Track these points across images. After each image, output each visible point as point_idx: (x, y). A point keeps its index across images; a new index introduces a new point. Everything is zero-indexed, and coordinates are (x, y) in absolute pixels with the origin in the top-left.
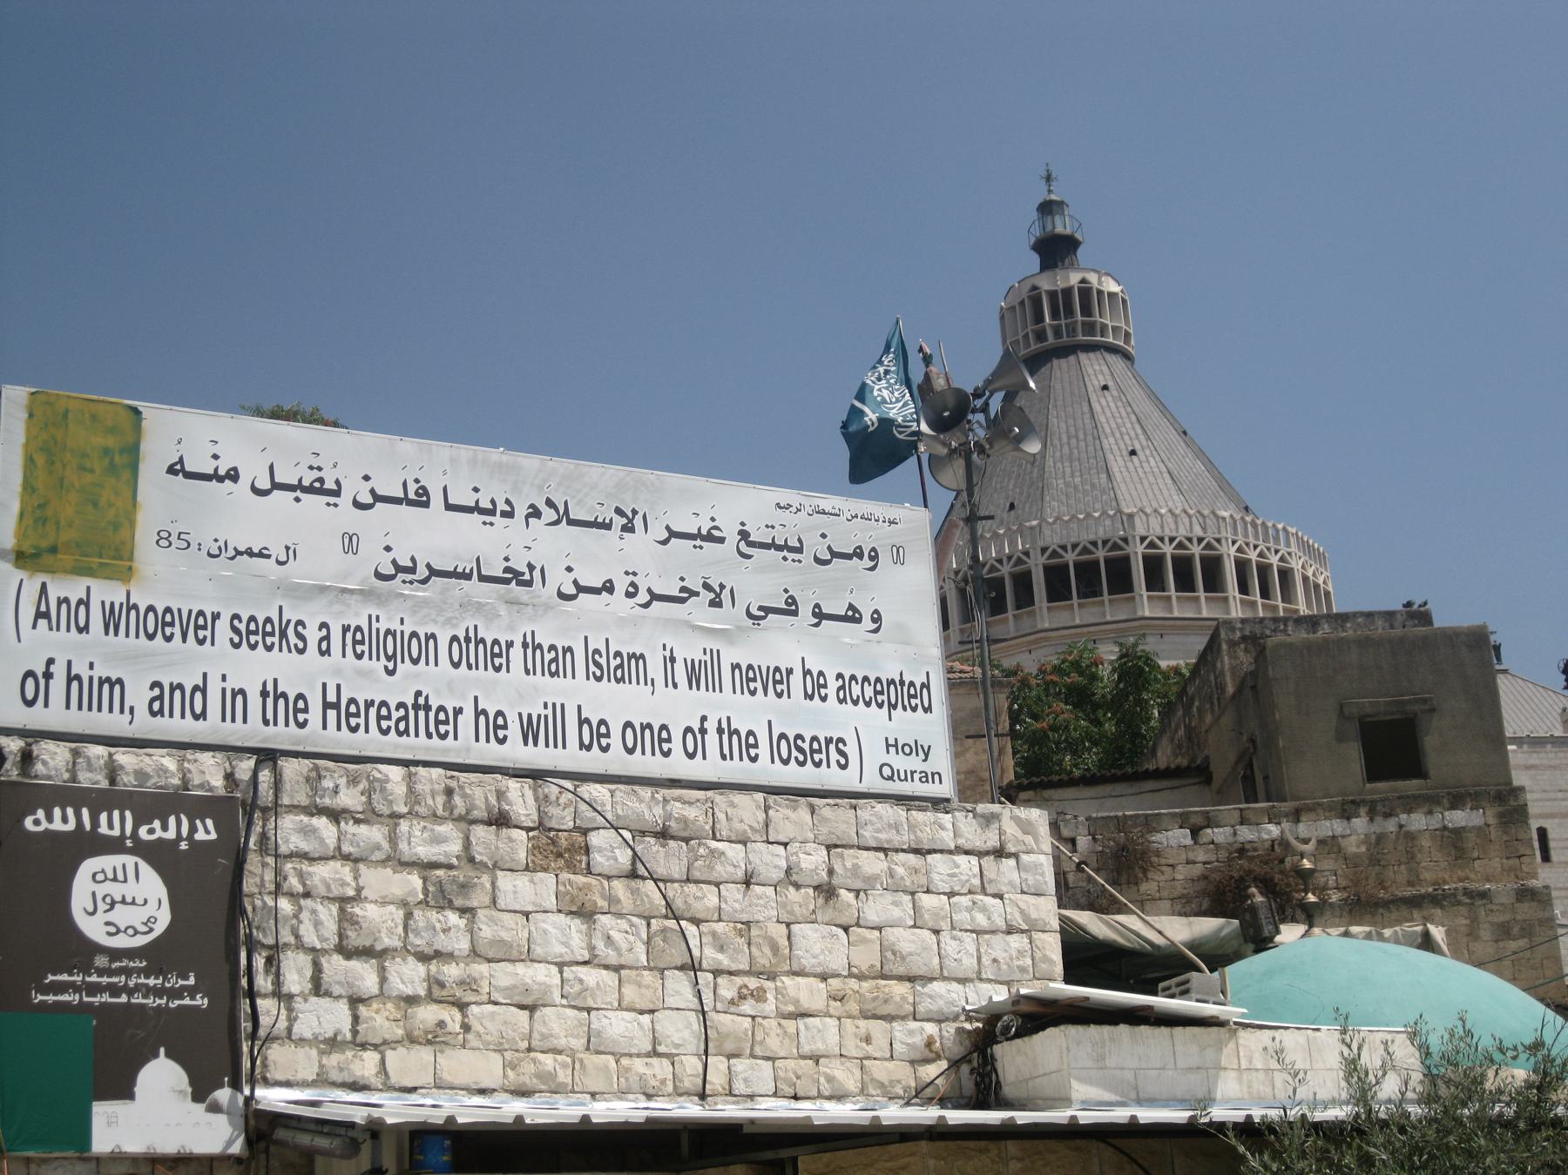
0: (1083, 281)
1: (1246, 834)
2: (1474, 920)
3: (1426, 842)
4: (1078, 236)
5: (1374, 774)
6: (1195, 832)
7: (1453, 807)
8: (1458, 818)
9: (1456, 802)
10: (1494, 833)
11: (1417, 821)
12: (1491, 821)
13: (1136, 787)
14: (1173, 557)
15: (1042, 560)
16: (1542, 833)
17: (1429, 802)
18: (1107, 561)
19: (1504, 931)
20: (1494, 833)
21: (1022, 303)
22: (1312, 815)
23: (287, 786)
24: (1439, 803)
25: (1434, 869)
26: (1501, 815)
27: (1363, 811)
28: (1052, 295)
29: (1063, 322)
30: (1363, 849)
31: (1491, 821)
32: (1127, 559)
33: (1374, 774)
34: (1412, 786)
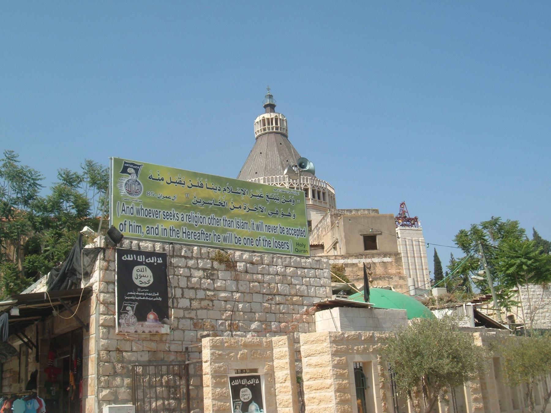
1: (337, 262)
3: (378, 265)
9: (385, 255)
11: (376, 260)
17: (379, 255)
26: (395, 259)
27: (364, 257)
28: (268, 119)
29: (271, 126)
34: (374, 251)
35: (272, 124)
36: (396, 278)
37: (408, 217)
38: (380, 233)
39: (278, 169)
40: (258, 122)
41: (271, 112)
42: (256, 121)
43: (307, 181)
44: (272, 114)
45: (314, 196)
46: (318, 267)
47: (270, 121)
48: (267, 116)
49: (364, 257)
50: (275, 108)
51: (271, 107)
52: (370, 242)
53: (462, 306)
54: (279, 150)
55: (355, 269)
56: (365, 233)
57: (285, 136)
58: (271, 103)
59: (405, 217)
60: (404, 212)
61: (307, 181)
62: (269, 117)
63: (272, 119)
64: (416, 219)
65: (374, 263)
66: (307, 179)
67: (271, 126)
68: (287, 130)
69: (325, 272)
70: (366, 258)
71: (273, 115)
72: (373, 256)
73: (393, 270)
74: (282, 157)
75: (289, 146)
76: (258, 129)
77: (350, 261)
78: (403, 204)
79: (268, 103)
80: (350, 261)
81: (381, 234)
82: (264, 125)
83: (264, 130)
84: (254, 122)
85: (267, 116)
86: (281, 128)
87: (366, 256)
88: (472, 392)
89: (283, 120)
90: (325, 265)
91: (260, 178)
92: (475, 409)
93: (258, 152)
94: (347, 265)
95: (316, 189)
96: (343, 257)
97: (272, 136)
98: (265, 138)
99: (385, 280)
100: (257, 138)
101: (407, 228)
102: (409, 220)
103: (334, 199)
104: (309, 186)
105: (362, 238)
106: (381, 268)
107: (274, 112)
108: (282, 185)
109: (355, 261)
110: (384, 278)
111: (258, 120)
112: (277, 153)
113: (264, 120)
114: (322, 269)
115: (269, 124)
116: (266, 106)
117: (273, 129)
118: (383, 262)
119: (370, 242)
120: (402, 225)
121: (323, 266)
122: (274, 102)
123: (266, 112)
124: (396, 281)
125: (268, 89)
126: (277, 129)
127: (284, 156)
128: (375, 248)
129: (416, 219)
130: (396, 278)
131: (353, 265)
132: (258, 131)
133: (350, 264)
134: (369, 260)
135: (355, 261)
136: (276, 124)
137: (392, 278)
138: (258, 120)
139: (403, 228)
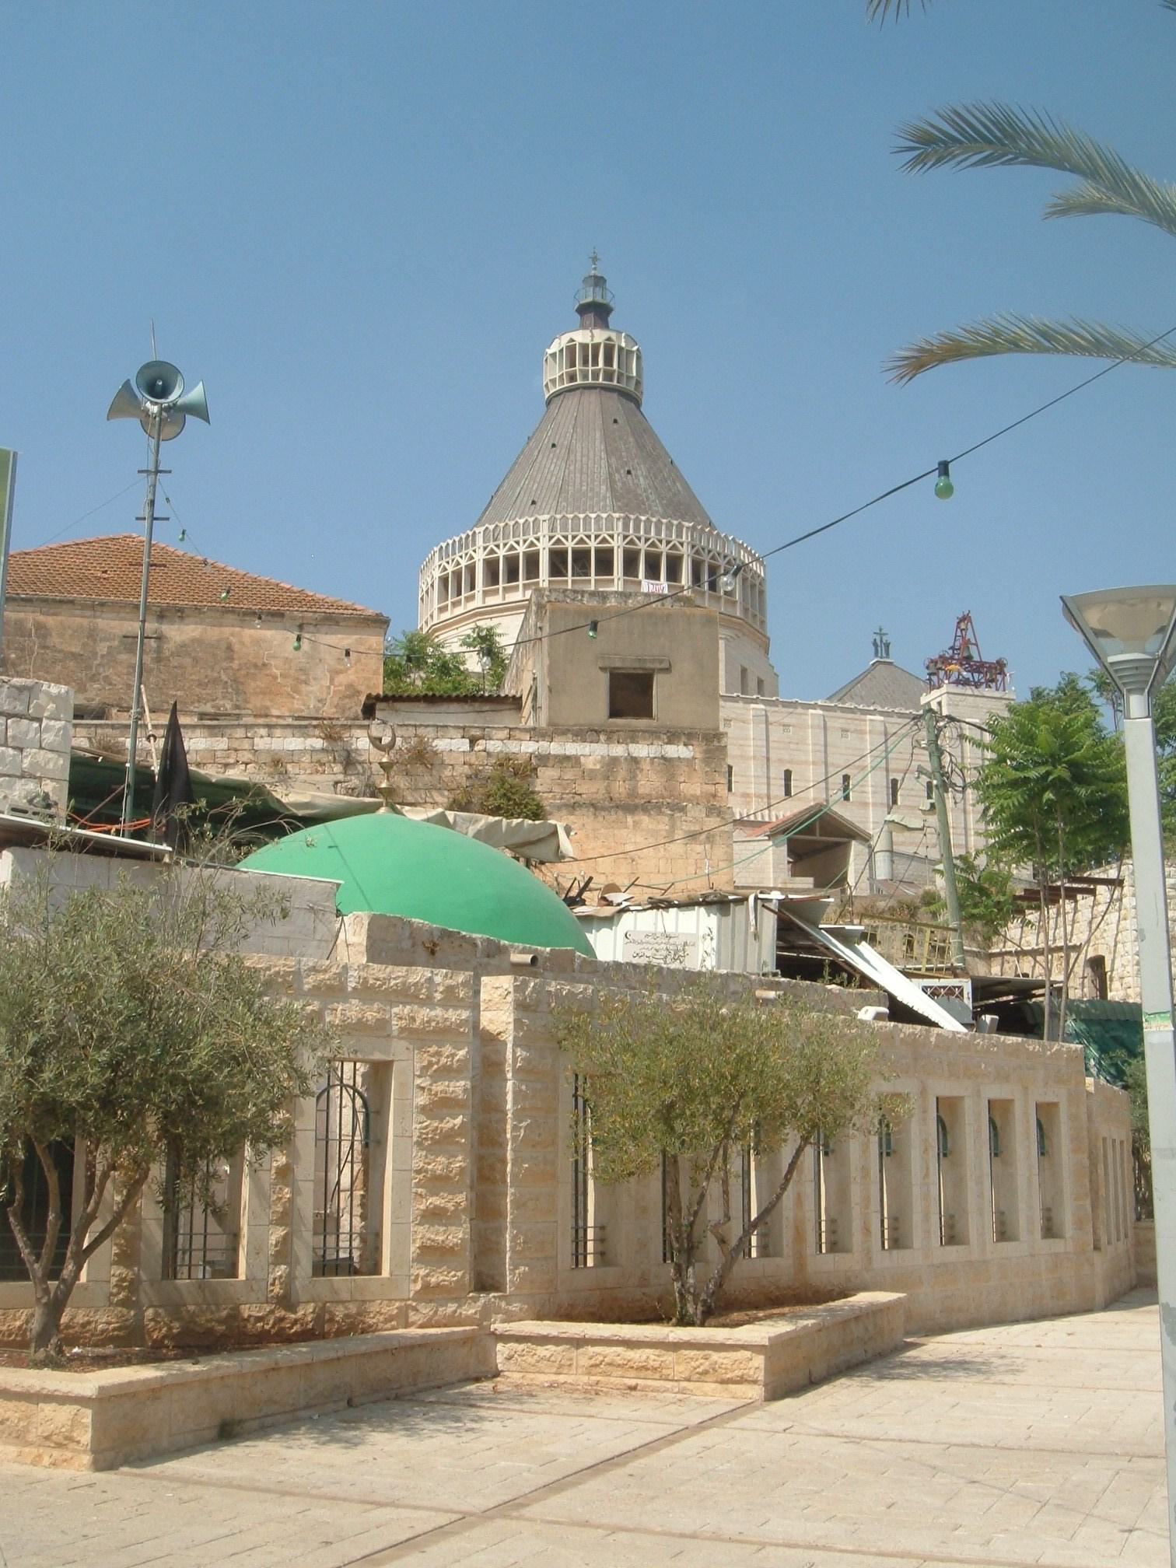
0: (609, 339)
1: (513, 747)
2: (673, 827)
3: (646, 766)
4: (612, 304)
5: (614, 713)
6: (473, 741)
7: (670, 742)
8: (675, 751)
9: (673, 737)
10: (698, 765)
11: (641, 750)
12: (698, 756)
13: (467, 707)
14: (668, 556)
15: (549, 545)
16: (730, 768)
17: (653, 735)
18: (597, 551)
19: (692, 836)
20: (698, 765)
21: (561, 351)
22: (563, 738)
23: (729, 704)
24: (659, 738)
25: (649, 783)
26: (706, 752)
27: (602, 737)
28: (584, 347)
29: (590, 368)
30: (598, 767)
31: (698, 756)
32: (611, 550)
33: (614, 713)
34: (642, 723)
35: (595, 362)
36: (695, 812)
37: (976, 658)
38: (665, 665)
39: (598, 494)
40: (553, 355)
41: (596, 326)
42: (550, 351)
43: (679, 535)
44: (597, 332)
45: (696, 578)
46: (20, 708)
47: (589, 353)
48: (581, 337)
49: (602, 737)
50: (611, 319)
51: (597, 313)
52: (631, 694)
53: (746, 899)
54: (606, 438)
55: (569, 775)
56: (618, 664)
57: (632, 398)
58: (599, 299)
59: (969, 658)
60: (967, 643)
61: (679, 535)
62: (588, 340)
63: (596, 347)
64: (999, 667)
65: (635, 761)
66: (680, 527)
67: (590, 368)
68: (638, 383)
69: (48, 729)
70: (609, 740)
71: (600, 336)
72: (633, 737)
73: (692, 787)
74: (613, 460)
75: (643, 434)
76: (553, 373)
77: (555, 748)
78: (965, 618)
79: (590, 299)
80: (555, 748)
81: (668, 670)
82: (573, 365)
83: (572, 378)
84: (544, 353)
85: (581, 337)
86: (620, 375)
87: (611, 736)
88: (418, 1185)
89: (629, 352)
90: (51, 706)
91: (541, 518)
92: (423, 1248)
93: (547, 442)
94: (544, 759)
95: (707, 558)
96: (536, 734)
97: (593, 397)
98: (572, 400)
99: (661, 813)
100: (549, 402)
101: (968, 690)
102: (979, 667)
103: (761, 593)
104: (685, 551)
105: (605, 678)
106: (653, 777)
107: (605, 325)
108: (604, 540)
109: (572, 748)
110: (658, 808)
111: (554, 348)
112: (599, 445)
113: (571, 349)
114: (39, 720)
115: (585, 363)
116: (583, 310)
117: (596, 375)
118: (663, 758)
119: (631, 694)
120: (957, 682)
121: (43, 708)
122: (609, 296)
123: (583, 327)
124: (696, 820)
125: (595, 259)
126: (609, 376)
127: (621, 457)
128: (646, 711)
129: (999, 667)
130: (695, 812)
131: (565, 760)
132: (553, 381)
133: (556, 756)
134: (618, 750)
135: (572, 748)
136: (608, 361)
137: (683, 810)
138: (554, 348)
139: (960, 689)
